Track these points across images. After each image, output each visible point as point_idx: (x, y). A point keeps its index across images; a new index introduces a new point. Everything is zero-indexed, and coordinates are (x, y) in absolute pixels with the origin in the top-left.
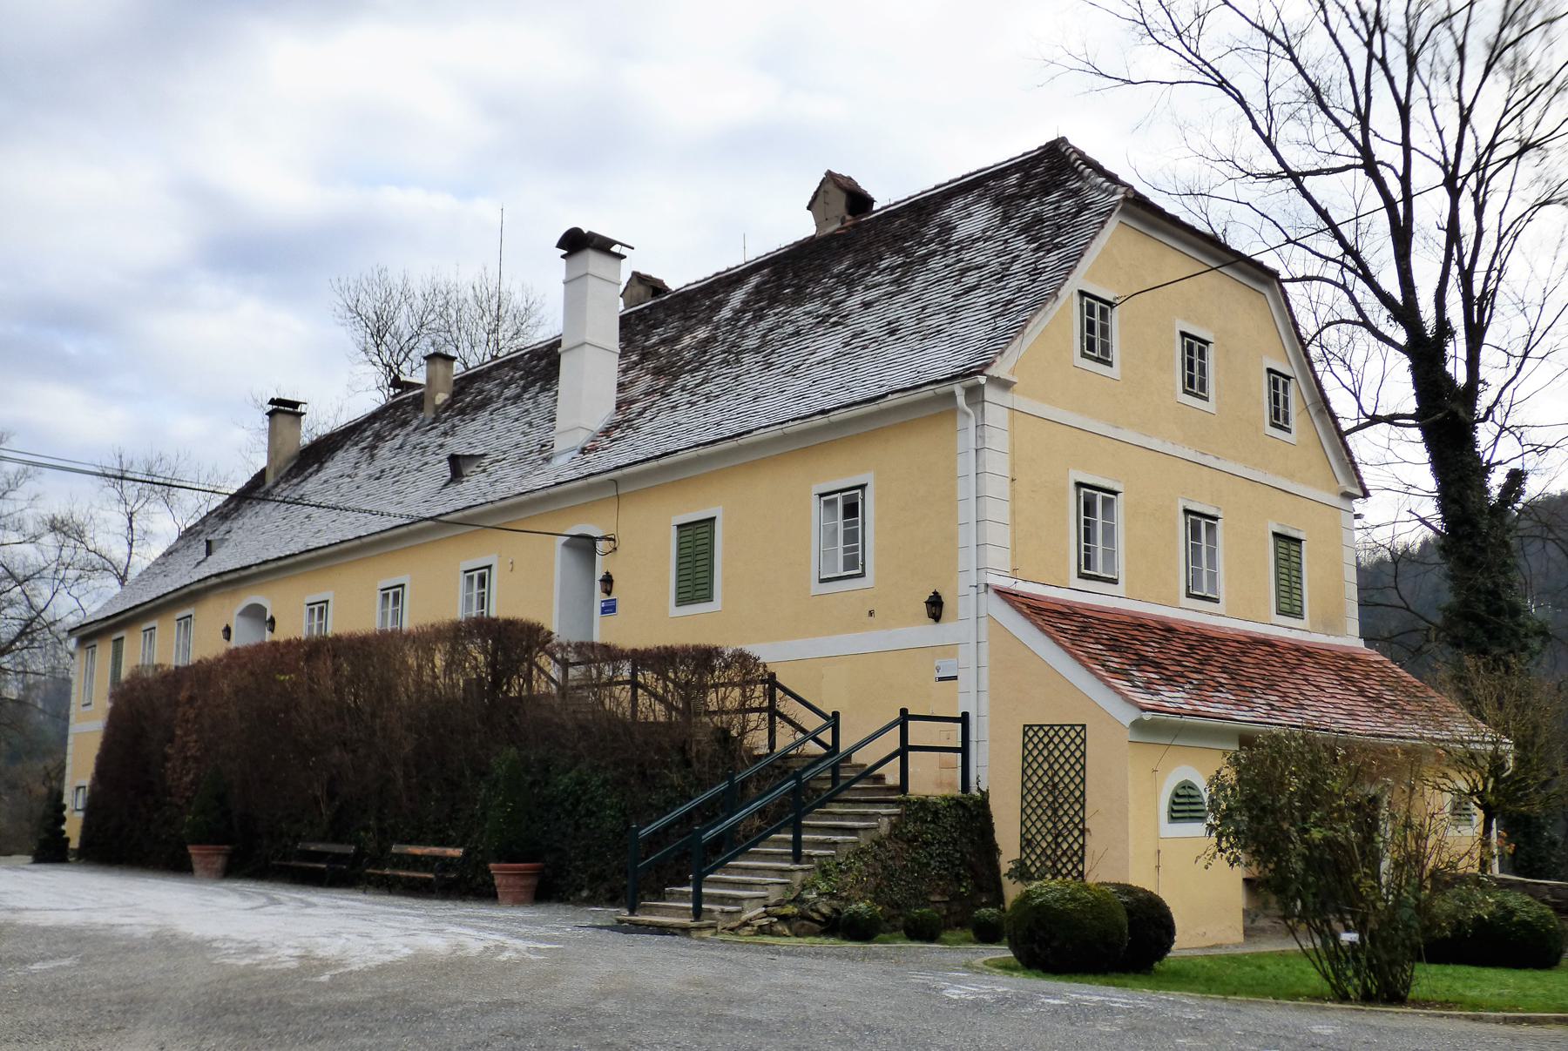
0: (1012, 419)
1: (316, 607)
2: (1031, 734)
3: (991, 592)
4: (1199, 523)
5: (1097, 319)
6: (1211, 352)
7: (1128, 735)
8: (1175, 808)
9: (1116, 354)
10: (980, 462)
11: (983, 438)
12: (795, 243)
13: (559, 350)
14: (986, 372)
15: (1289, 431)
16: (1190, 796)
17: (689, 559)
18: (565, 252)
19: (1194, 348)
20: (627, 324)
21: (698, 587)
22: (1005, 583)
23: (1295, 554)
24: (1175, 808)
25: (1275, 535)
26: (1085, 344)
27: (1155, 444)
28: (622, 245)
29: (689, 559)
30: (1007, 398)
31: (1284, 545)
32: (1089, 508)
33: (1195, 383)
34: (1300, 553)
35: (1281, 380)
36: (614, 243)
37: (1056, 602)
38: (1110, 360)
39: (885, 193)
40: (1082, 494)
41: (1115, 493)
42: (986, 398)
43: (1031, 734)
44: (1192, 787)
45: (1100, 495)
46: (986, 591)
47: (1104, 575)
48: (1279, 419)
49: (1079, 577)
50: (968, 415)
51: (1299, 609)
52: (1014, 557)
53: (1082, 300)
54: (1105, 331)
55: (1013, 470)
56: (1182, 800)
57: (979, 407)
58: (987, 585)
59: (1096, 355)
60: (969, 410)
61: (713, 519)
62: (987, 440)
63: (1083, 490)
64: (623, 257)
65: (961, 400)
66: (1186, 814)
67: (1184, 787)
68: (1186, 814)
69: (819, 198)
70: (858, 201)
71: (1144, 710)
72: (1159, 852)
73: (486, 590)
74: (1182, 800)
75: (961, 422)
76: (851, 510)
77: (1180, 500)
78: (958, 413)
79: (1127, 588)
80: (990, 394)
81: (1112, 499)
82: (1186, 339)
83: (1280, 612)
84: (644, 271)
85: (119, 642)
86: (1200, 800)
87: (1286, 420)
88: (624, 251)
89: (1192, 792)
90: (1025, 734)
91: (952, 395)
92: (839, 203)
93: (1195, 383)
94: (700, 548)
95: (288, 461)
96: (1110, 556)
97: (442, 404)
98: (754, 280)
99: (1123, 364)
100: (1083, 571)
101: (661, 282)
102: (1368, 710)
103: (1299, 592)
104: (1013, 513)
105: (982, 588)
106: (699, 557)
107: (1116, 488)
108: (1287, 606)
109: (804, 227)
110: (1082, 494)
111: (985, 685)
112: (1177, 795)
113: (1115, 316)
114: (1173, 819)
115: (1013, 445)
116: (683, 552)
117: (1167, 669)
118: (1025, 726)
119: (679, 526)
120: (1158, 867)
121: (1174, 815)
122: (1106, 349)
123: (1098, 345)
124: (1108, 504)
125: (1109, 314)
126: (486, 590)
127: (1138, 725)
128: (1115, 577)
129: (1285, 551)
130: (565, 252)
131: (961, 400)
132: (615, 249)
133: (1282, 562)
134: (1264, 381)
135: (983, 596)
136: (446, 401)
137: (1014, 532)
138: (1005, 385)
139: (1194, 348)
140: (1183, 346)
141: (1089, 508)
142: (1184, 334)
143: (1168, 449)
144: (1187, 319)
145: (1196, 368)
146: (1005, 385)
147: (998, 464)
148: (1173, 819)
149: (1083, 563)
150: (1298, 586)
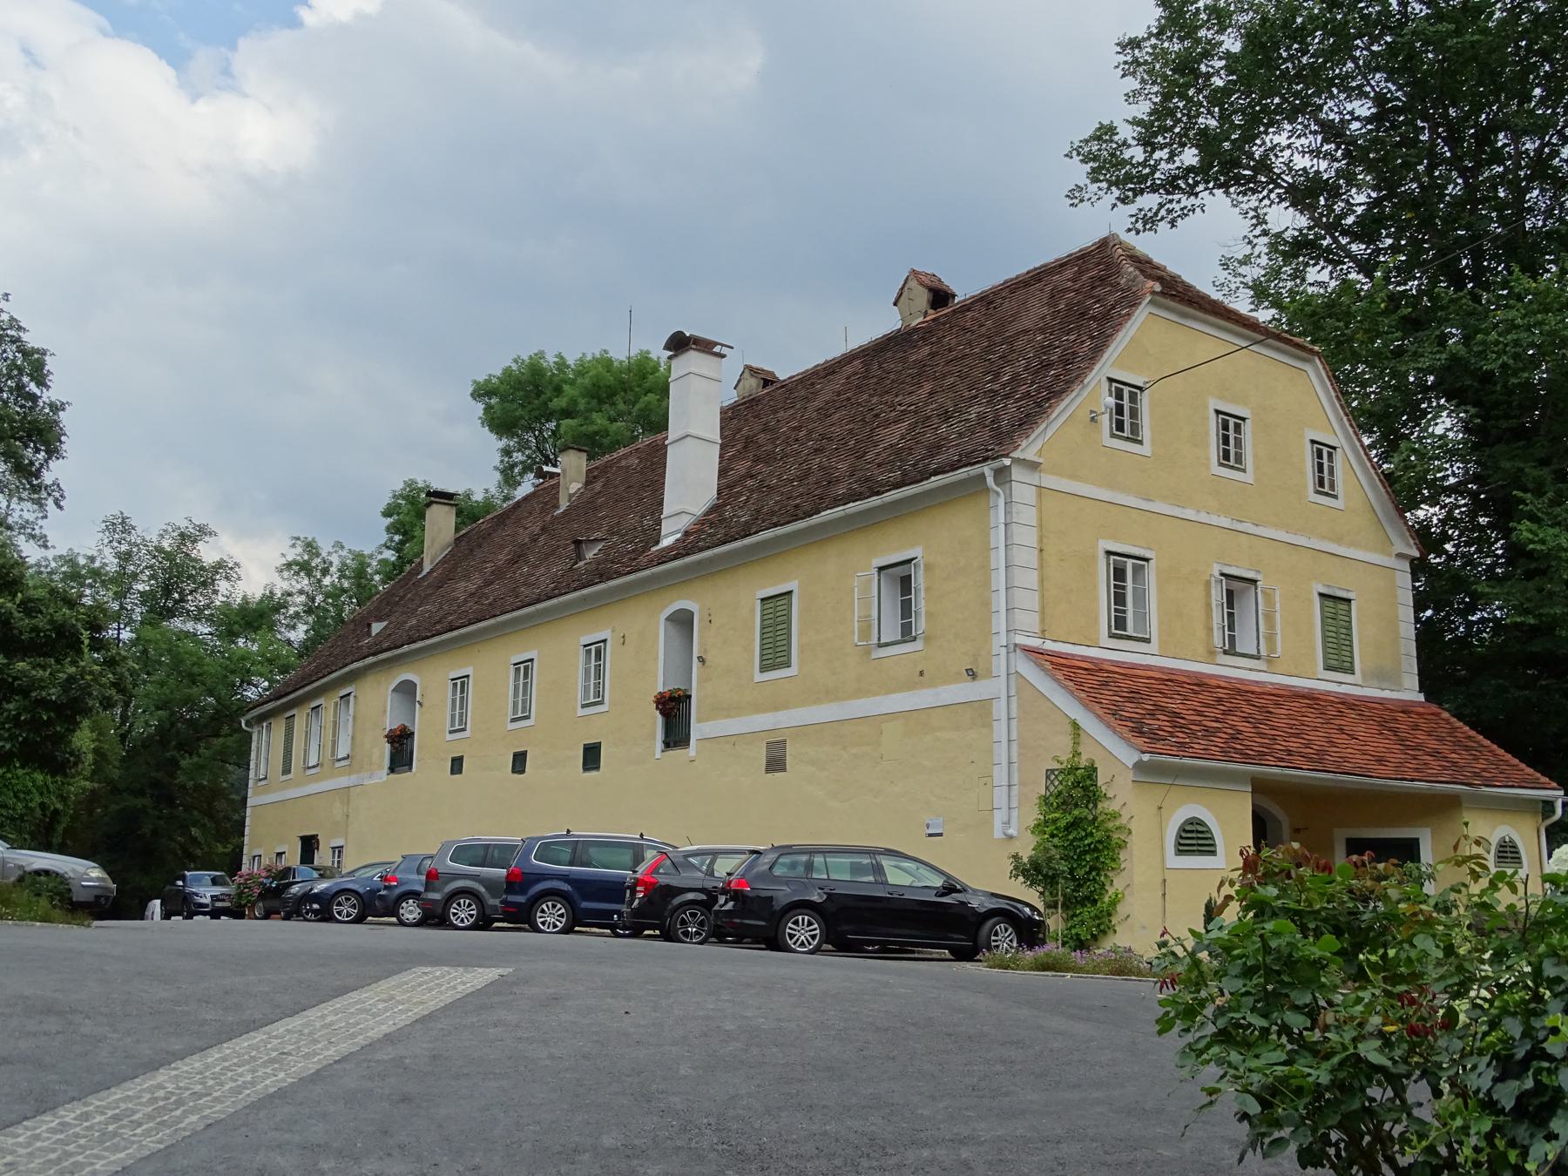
0: (1039, 495)
1: (459, 681)
2: (1053, 777)
3: (1018, 651)
4: (1236, 588)
5: (1126, 402)
6: (1247, 428)
7: (1131, 776)
8: (1182, 842)
9: (1146, 433)
10: (1009, 534)
11: (1011, 513)
12: (884, 336)
13: (666, 442)
14: (1011, 455)
15: (1335, 497)
16: (1202, 832)
17: (770, 629)
18: (671, 353)
19: (1229, 427)
20: (730, 416)
21: (778, 654)
22: (1035, 643)
23: (1344, 613)
24: (1182, 842)
25: (1321, 595)
26: (1114, 426)
27: (1190, 514)
28: (723, 345)
29: (770, 629)
30: (1034, 478)
31: (1331, 604)
32: (1119, 574)
33: (1230, 455)
34: (1350, 611)
35: (1325, 450)
36: (716, 344)
37: (1084, 659)
38: (1140, 438)
39: (964, 289)
40: (1111, 562)
41: (1147, 560)
42: (1013, 478)
43: (1053, 777)
44: (1201, 823)
45: (1130, 562)
46: (1015, 651)
47: (1135, 635)
48: (1324, 483)
49: (1110, 637)
50: (998, 494)
51: (1349, 665)
52: (1043, 621)
53: (1111, 386)
54: (1134, 413)
55: (1041, 540)
56: (1189, 835)
57: (1008, 485)
58: (1016, 645)
59: (1125, 435)
60: (999, 489)
61: (790, 593)
62: (1014, 515)
63: (1112, 557)
64: (723, 356)
65: (990, 481)
66: (1195, 848)
67: (1192, 824)
68: (1195, 848)
69: (904, 295)
70: (940, 297)
71: (1143, 752)
72: (1165, 881)
73: (602, 662)
74: (1189, 835)
75: (992, 497)
76: (906, 584)
77: (1215, 565)
78: (991, 494)
79: (1160, 647)
80: (1017, 474)
81: (1144, 566)
82: (1221, 416)
83: (1328, 668)
84: (755, 365)
85: (291, 719)
86: (1210, 836)
87: (1332, 486)
88: (725, 351)
89: (1200, 828)
90: (1048, 777)
91: (982, 476)
92: (922, 298)
93: (1230, 455)
94: (779, 619)
95: (443, 549)
96: (1142, 618)
97: (576, 493)
98: (849, 369)
99: (1153, 441)
100: (1114, 631)
101: (772, 374)
102: (1403, 756)
103: (1348, 648)
104: (1042, 581)
105: (1012, 647)
106: (779, 627)
107: (1148, 555)
108: (1335, 662)
109: (887, 321)
110: (1111, 562)
111: (1014, 736)
112: (1185, 831)
113: (1145, 400)
114: (1179, 852)
115: (1040, 519)
116: (765, 623)
117: (1183, 718)
118: (1047, 770)
119: (762, 600)
120: (1164, 895)
121: (1181, 848)
122: (1135, 428)
123: (1127, 426)
124: (1138, 570)
125: (1139, 397)
126: (602, 662)
127: (1139, 766)
128: (1148, 636)
129: (1333, 611)
130: (671, 353)
131: (990, 481)
132: (717, 349)
133: (1330, 620)
134: (1308, 452)
135: (1012, 655)
136: (579, 489)
137: (1042, 596)
138: (1033, 466)
139: (1229, 427)
140: (1218, 423)
141: (1119, 574)
142: (1218, 412)
143: (1203, 517)
144: (1221, 397)
145: (1232, 442)
146: (1033, 466)
147: (1027, 537)
148: (1179, 852)
149: (1113, 623)
150: (1347, 643)
